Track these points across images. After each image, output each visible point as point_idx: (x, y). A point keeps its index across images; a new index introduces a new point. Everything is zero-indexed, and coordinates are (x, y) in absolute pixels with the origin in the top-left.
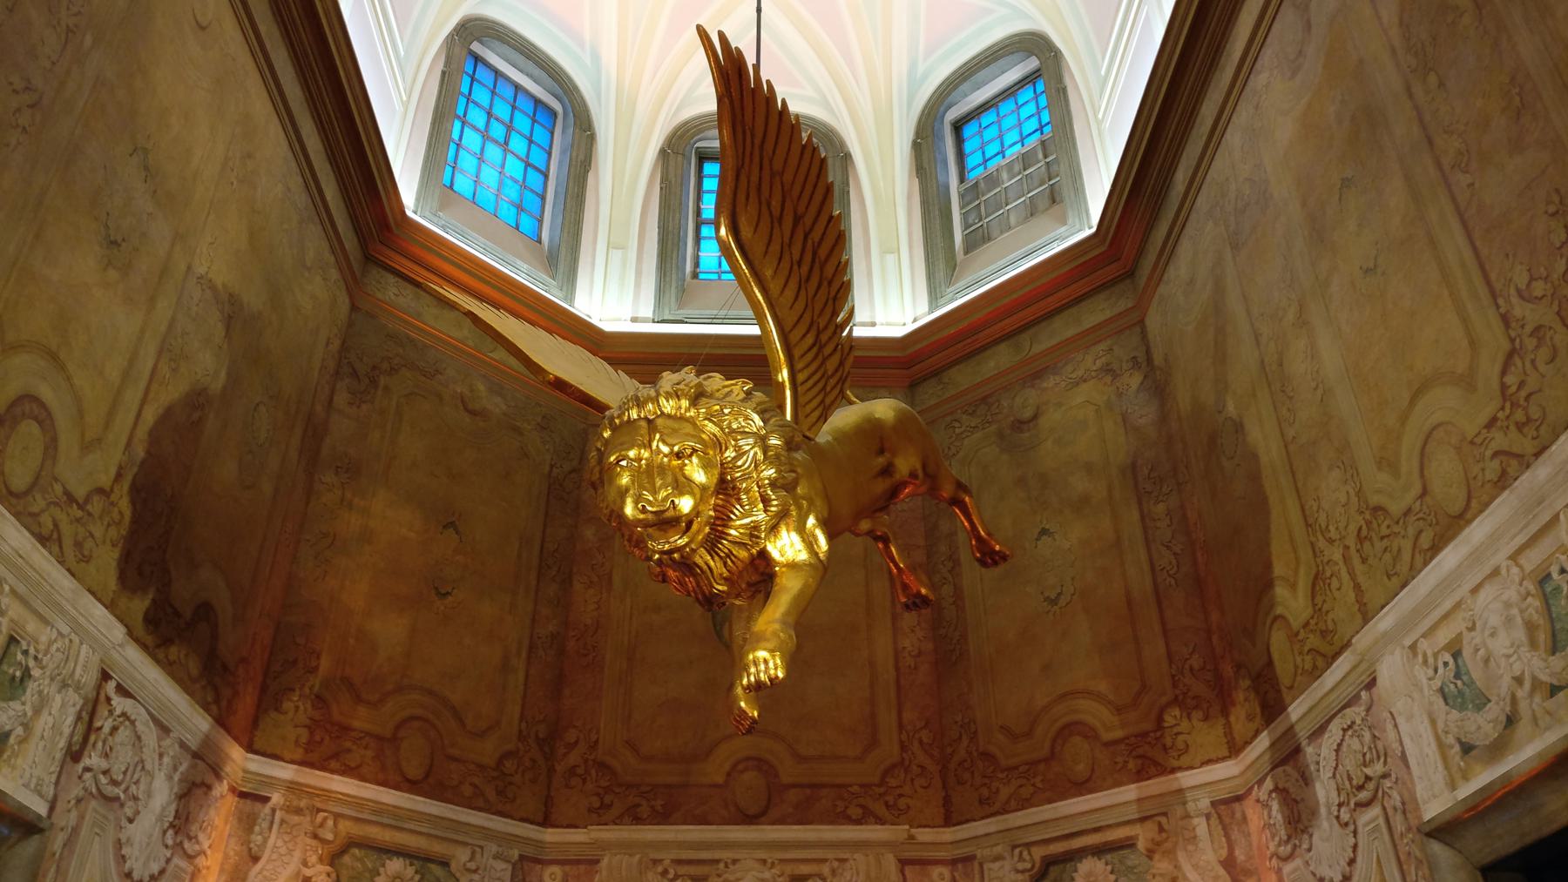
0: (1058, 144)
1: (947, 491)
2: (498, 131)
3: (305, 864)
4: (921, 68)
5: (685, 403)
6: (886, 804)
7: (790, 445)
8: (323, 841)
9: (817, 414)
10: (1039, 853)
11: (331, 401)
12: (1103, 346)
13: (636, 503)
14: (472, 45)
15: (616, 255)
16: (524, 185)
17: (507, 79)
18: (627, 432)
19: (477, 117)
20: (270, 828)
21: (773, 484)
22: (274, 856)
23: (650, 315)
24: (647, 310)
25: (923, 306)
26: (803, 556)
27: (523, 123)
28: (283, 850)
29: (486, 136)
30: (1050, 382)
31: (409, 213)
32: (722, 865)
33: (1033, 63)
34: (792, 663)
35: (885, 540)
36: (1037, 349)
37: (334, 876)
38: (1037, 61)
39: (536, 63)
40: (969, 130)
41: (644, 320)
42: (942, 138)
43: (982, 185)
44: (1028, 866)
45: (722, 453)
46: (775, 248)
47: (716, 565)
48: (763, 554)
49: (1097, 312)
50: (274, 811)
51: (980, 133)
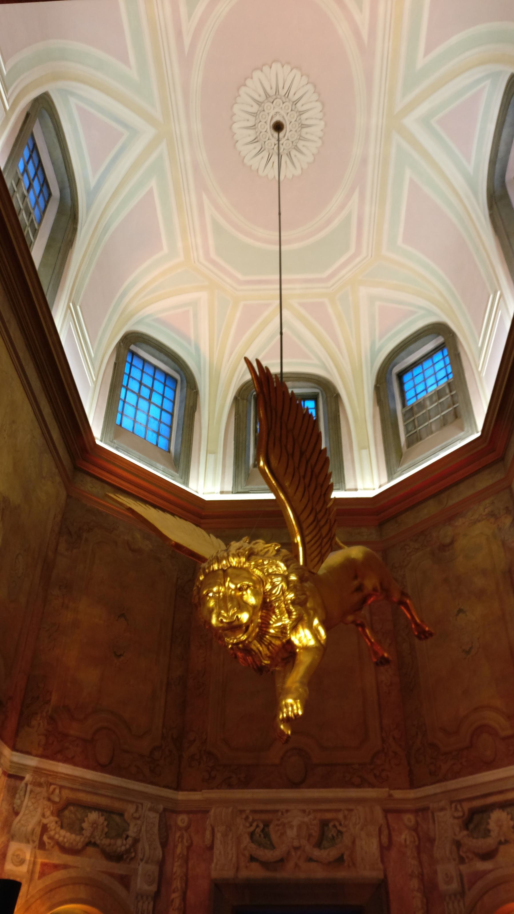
0: (456, 387)
1: (396, 597)
2: (145, 392)
3: (43, 816)
4: (378, 345)
5: (243, 560)
6: (375, 776)
7: (302, 579)
8: (54, 802)
9: (317, 559)
10: (467, 806)
11: (56, 549)
12: (487, 501)
13: (218, 617)
14: (132, 346)
15: (211, 457)
16: (160, 421)
17: (150, 364)
18: (214, 577)
19: (134, 385)
20: (25, 795)
21: (293, 602)
22: (27, 812)
23: (230, 489)
24: (229, 487)
25: (385, 479)
26: (312, 642)
27: (158, 387)
28: (32, 808)
29: (139, 395)
30: (459, 522)
31: (98, 442)
32: (280, 814)
33: (440, 340)
34: (305, 707)
35: (362, 626)
36: (451, 503)
37: (59, 823)
38: (442, 338)
39: (135, 486)
40: (407, 378)
41: (227, 493)
42: (391, 383)
43: (415, 409)
44: (460, 814)
45: (264, 586)
46: (290, 470)
47: (263, 649)
48: (290, 642)
49: (484, 481)
50: (26, 785)
51: (413, 378)
